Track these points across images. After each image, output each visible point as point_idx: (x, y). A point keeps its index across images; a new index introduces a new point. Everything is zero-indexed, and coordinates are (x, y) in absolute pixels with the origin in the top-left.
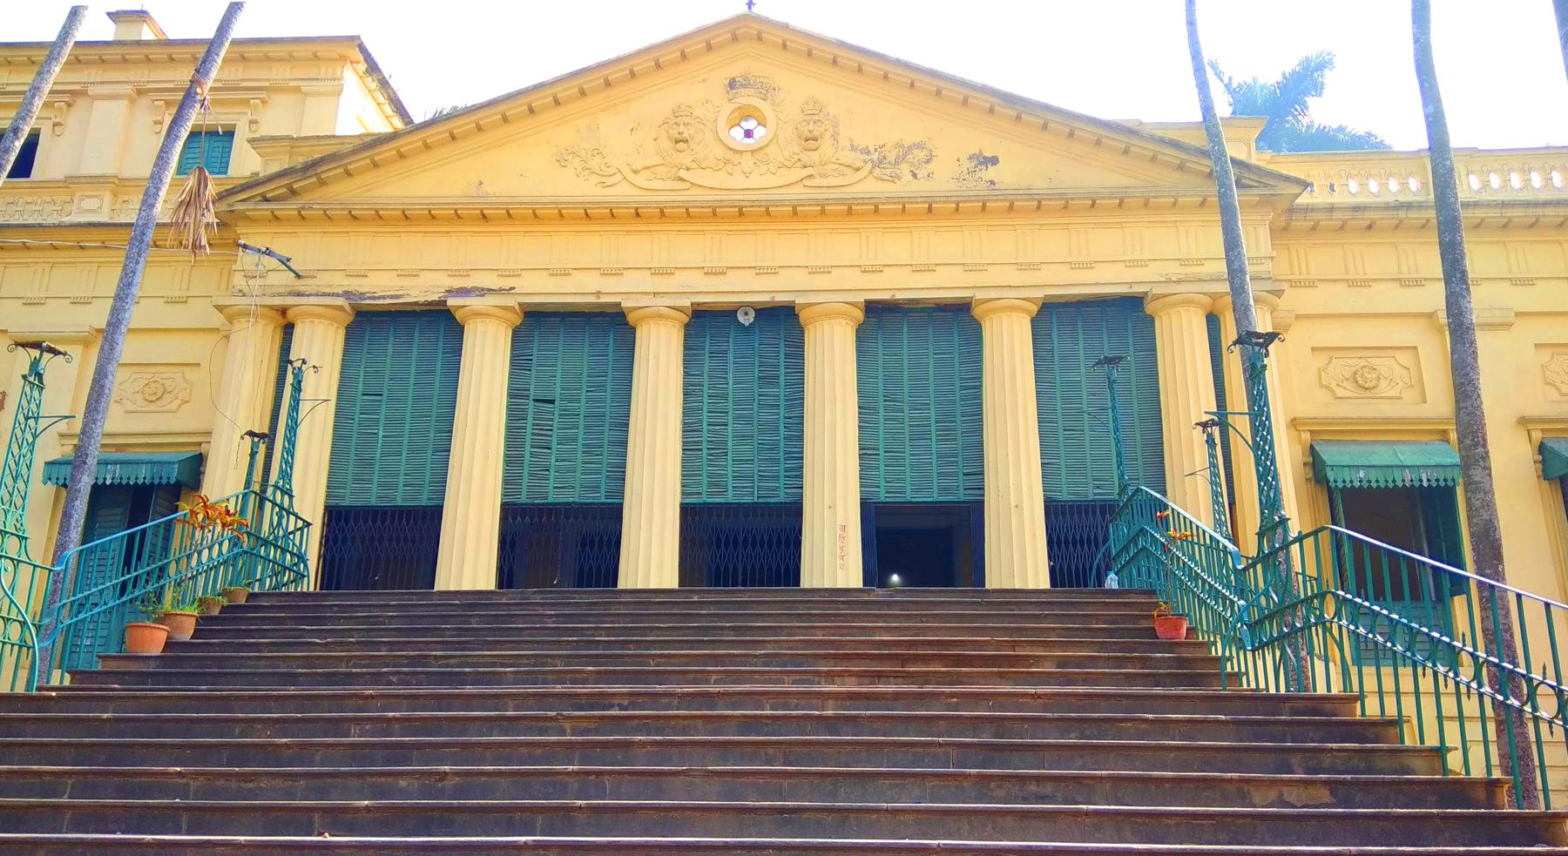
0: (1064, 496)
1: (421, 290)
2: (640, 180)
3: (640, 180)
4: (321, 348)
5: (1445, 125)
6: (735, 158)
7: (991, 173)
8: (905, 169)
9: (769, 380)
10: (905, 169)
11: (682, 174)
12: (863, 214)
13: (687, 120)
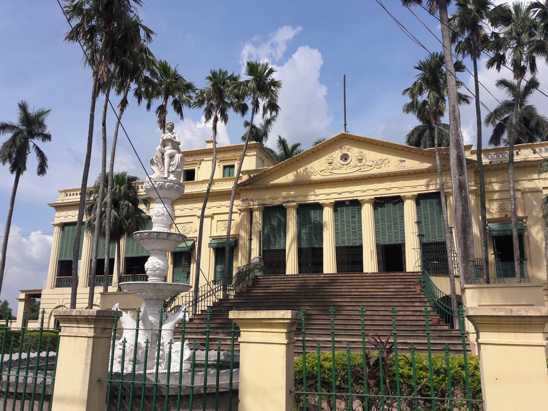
1: (277, 202)
2: (322, 173)
3: (322, 173)
4: (258, 216)
5: (440, 276)
6: (343, 166)
8: (383, 165)
9: (353, 217)
12: (300, 160)
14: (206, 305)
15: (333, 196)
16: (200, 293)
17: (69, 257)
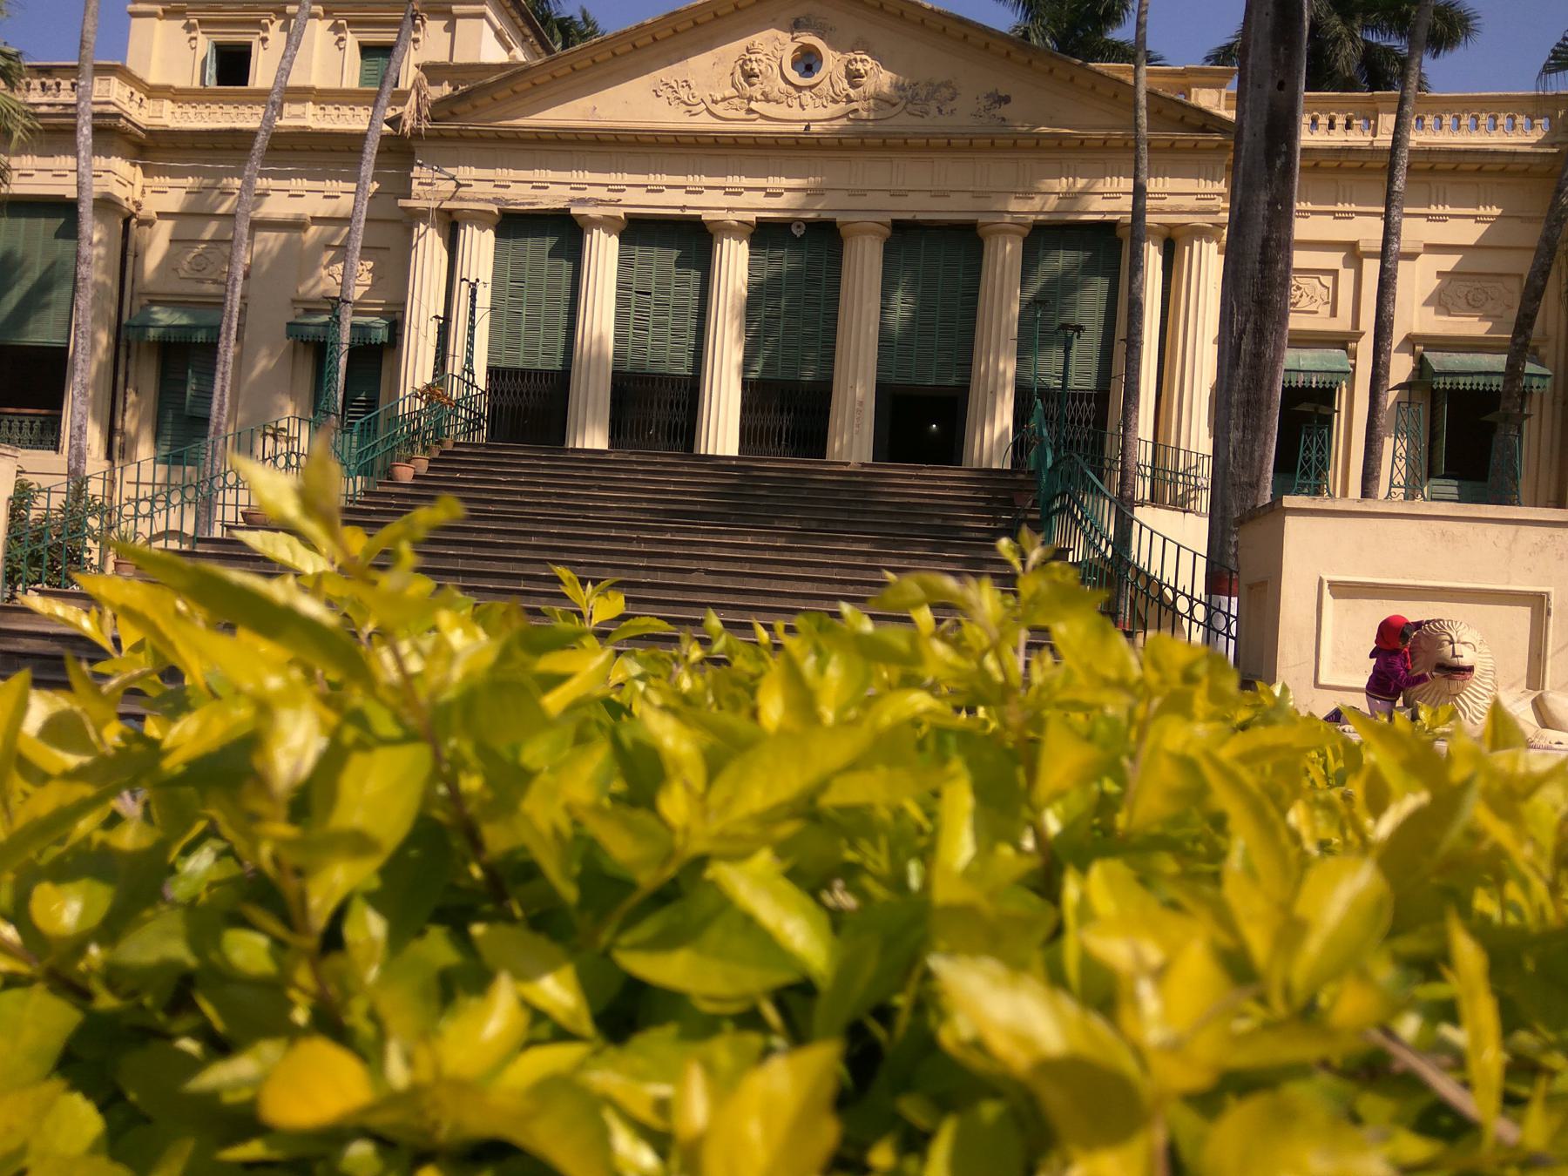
0: (893, 379)
2: (719, 109)
7: (1004, 110)
8: (933, 105)
10: (933, 105)
11: (753, 105)
13: (759, 56)
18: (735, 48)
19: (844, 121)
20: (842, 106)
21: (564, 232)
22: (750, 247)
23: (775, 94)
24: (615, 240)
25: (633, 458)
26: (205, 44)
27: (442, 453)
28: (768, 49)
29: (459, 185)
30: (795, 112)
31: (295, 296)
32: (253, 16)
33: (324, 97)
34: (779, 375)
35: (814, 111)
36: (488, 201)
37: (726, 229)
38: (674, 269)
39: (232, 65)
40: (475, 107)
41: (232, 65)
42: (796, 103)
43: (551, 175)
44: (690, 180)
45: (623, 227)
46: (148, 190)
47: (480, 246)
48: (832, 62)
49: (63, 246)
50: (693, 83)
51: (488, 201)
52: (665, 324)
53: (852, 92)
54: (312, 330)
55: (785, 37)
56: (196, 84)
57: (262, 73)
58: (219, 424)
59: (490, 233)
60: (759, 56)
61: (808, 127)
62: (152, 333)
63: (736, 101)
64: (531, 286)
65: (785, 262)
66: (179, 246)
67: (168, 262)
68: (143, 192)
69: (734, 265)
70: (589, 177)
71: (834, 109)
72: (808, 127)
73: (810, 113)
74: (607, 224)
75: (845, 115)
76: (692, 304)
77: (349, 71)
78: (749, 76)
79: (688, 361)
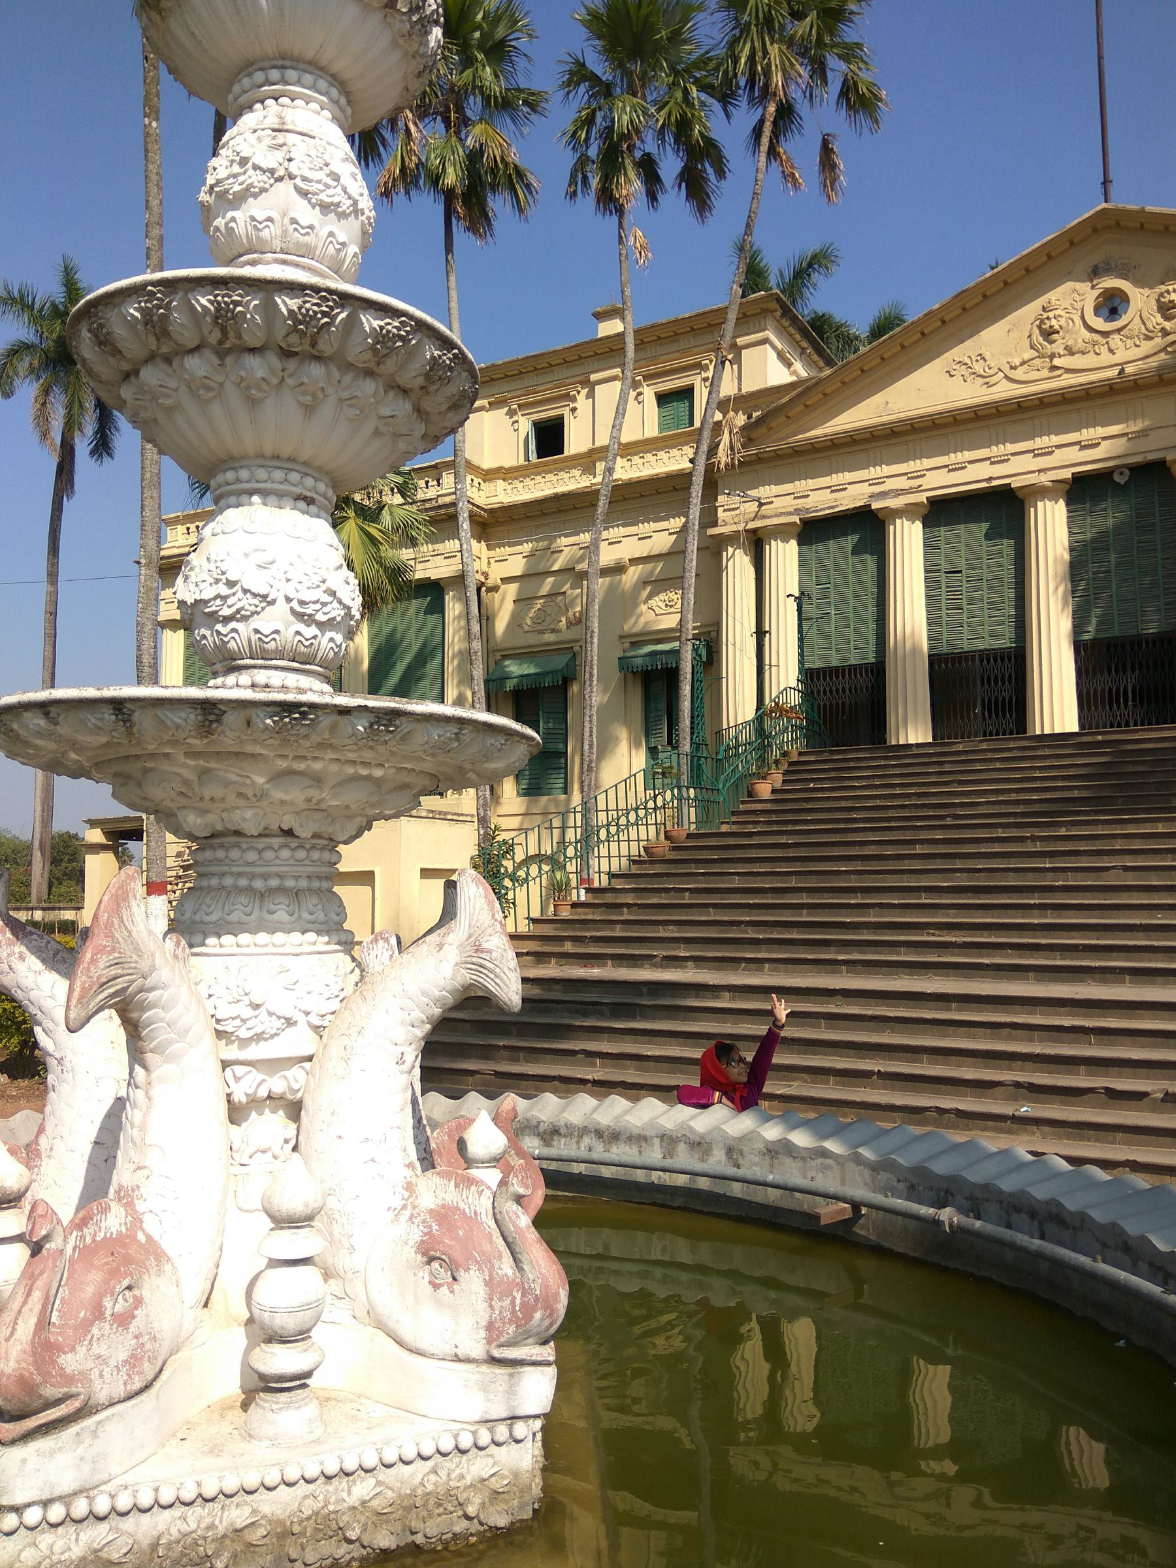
2: (1019, 374)
13: (1057, 312)
14: (624, 852)
15: (1060, 457)
16: (602, 816)
17: (984, 634)
18: (1031, 310)
19: (1163, 356)
20: (1158, 341)
21: (867, 527)
22: (1067, 505)
23: (1081, 345)
24: (918, 525)
25: (984, 746)
26: (525, 425)
27: (790, 764)
28: (1066, 303)
29: (761, 505)
30: (1106, 358)
31: (621, 633)
32: (562, 391)
33: (631, 450)
34: (1117, 632)
35: (1129, 352)
36: (789, 514)
37: (1039, 492)
38: (984, 543)
39: (549, 438)
40: (770, 429)
41: (549, 438)
42: (1104, 350)
43: (848, 476)
44: (995, 451)
45: (925, 511)
46: (492, 561)
47: (785, 557)
48: (1141, 300)
49: (432, 620)
50: (987, 355)
51: (789, 514)
52: (981, 599)
53: (1168, 325)
54: (639, 661)
55: (1084, 287)
56: (522, 462)
57: (576, 441)
58: (591, 762)
59: (793, 543)
60: (1057, 312)
61: (1122, 371)
62: (510, 685)
63: (1037, 362)
64: (837, 586)
65: (1110, 516)
66: (522, 604)
67: (516, 621)
68: (489, 563)
69: (1052, 529)
70: (887, 470)
71: (1147, 347)
72: (1122, 371)
73: (1121, 356)
74: (908, 512)
75: (1164, 350)
76: (1009, 574)
77: (644, 418)
78: (1048, 334)
79: (1009, 632)
